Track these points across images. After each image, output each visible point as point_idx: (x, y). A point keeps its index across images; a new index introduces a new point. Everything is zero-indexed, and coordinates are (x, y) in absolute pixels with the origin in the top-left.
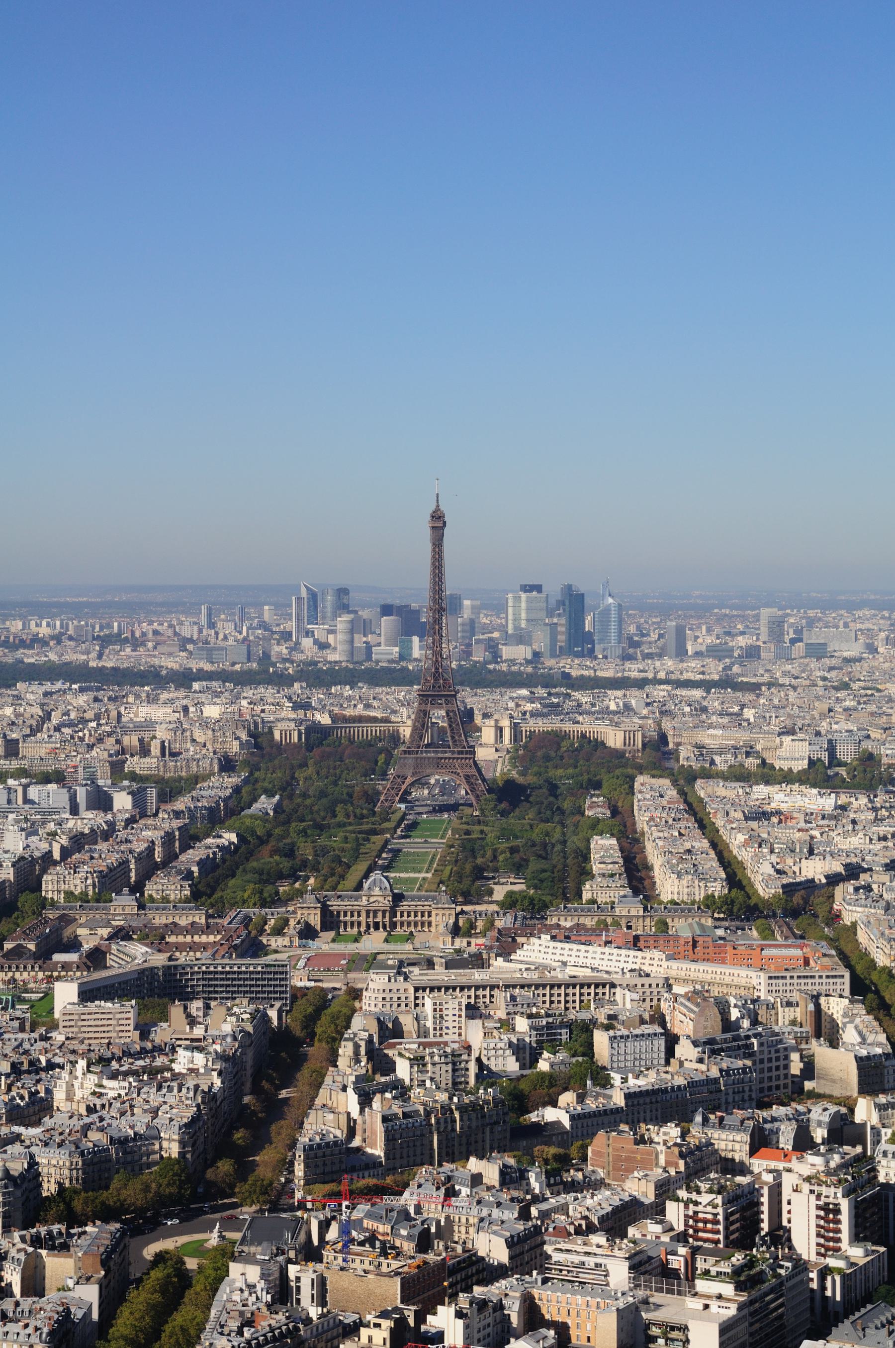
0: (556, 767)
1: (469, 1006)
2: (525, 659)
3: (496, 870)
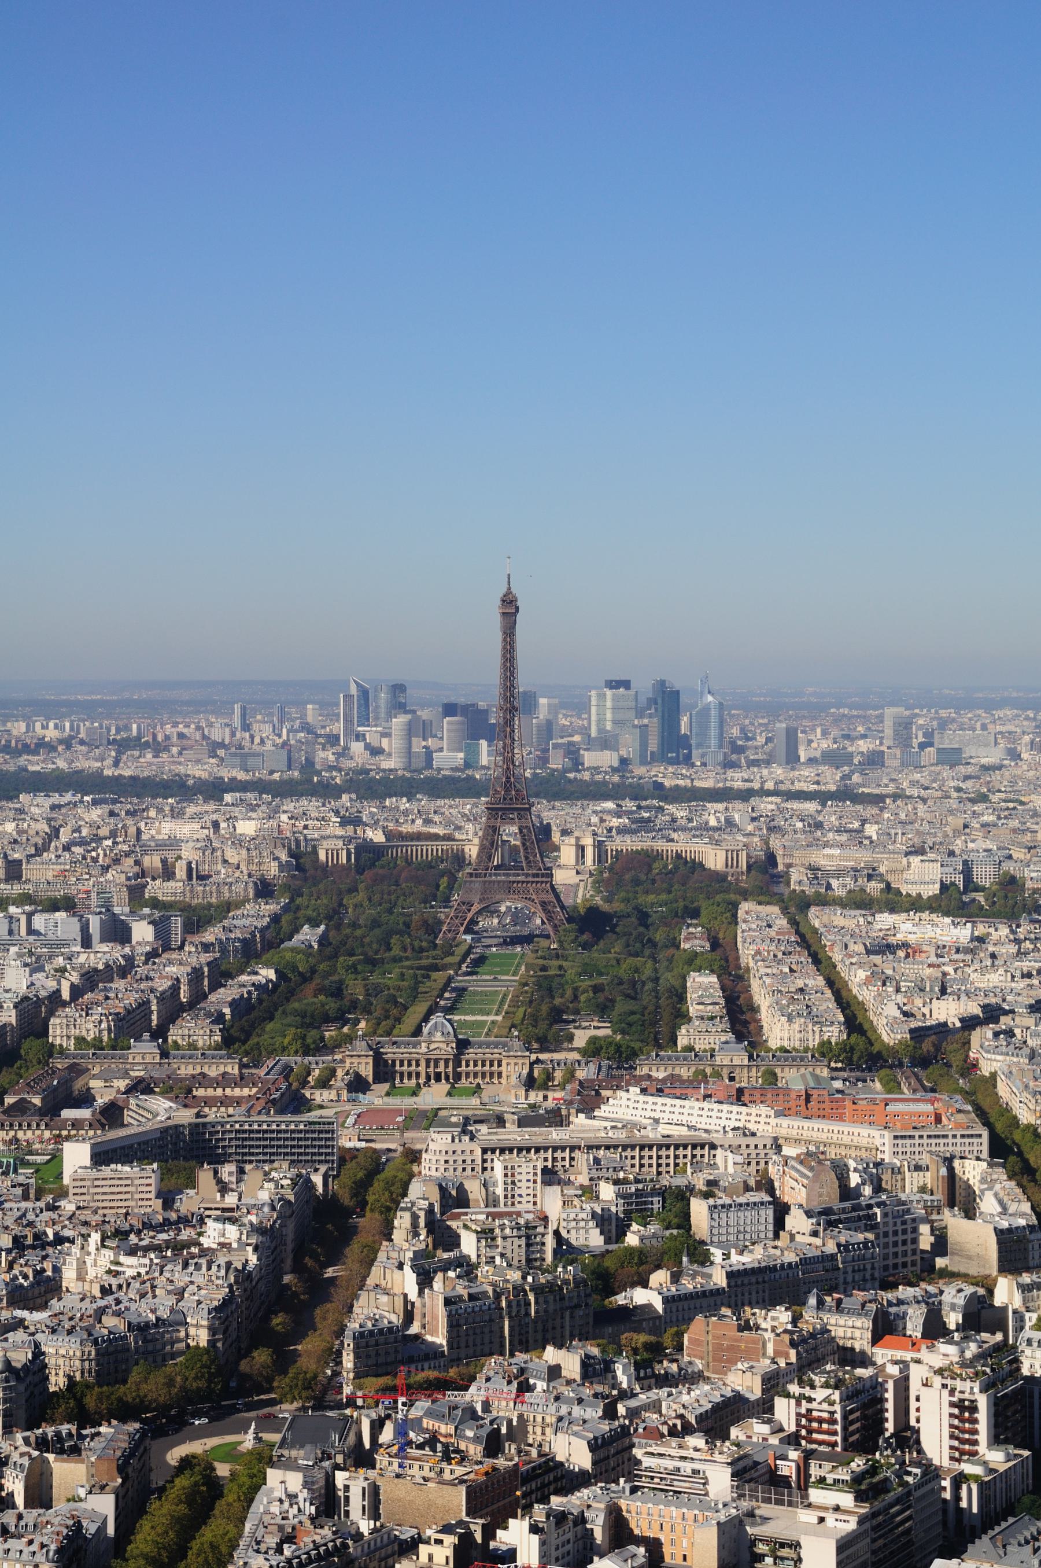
0: (647, 892)
1: (545, 1171)
2: (611, 767)
3: (577, 1012)
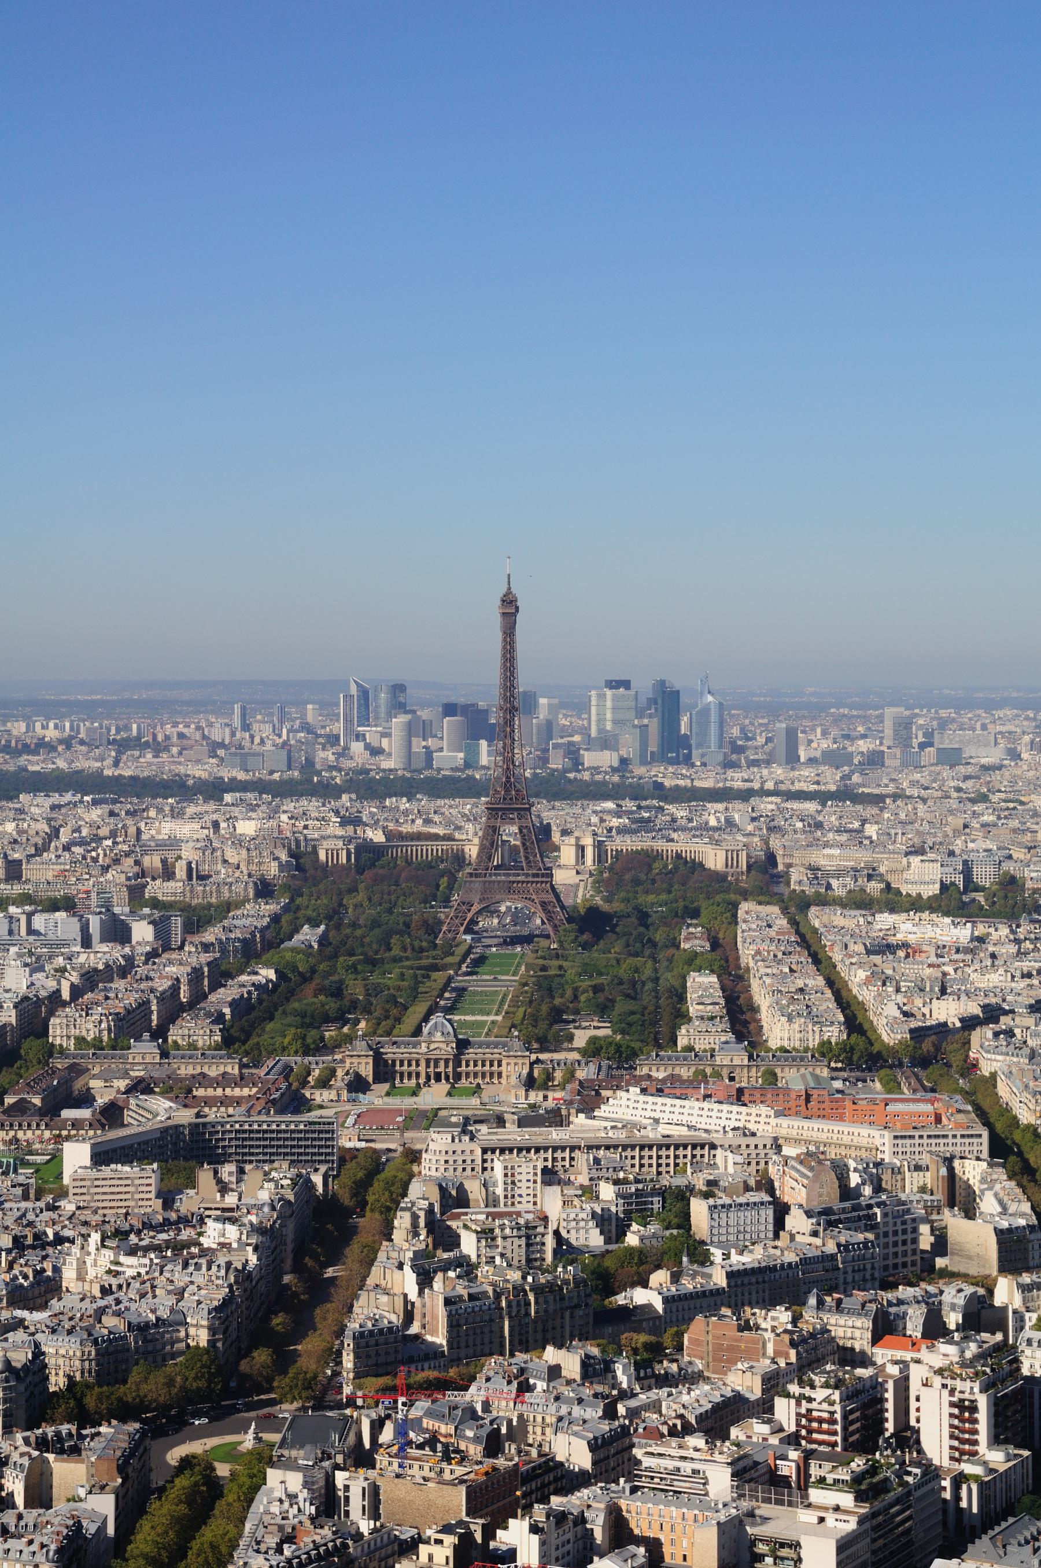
0: (647, 892)
1: (545, 1171)
2: (611, 767)
3: (577, 1012)
